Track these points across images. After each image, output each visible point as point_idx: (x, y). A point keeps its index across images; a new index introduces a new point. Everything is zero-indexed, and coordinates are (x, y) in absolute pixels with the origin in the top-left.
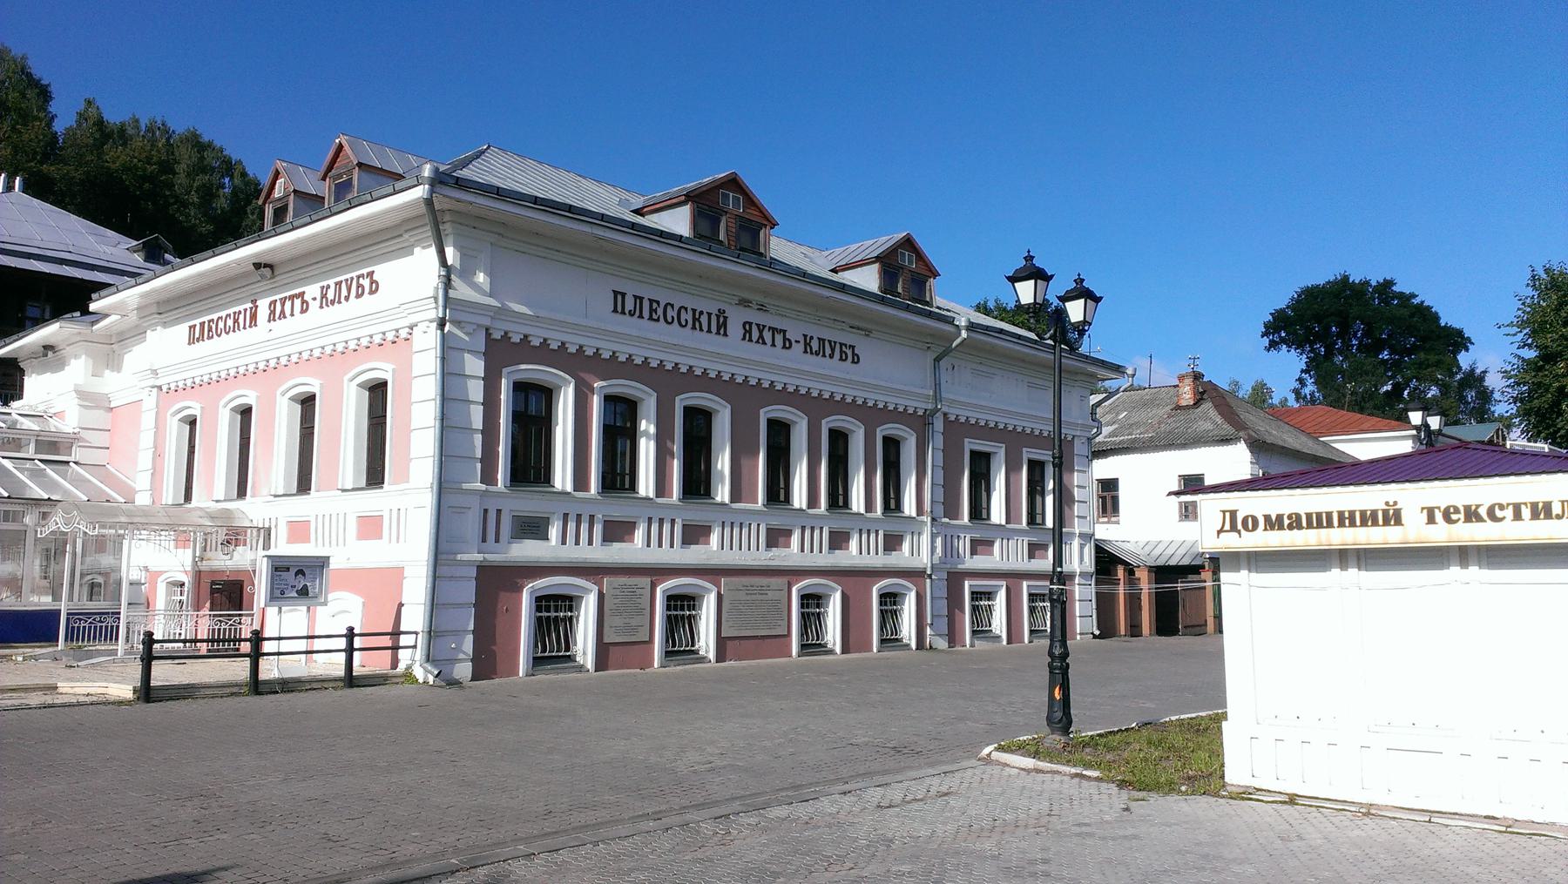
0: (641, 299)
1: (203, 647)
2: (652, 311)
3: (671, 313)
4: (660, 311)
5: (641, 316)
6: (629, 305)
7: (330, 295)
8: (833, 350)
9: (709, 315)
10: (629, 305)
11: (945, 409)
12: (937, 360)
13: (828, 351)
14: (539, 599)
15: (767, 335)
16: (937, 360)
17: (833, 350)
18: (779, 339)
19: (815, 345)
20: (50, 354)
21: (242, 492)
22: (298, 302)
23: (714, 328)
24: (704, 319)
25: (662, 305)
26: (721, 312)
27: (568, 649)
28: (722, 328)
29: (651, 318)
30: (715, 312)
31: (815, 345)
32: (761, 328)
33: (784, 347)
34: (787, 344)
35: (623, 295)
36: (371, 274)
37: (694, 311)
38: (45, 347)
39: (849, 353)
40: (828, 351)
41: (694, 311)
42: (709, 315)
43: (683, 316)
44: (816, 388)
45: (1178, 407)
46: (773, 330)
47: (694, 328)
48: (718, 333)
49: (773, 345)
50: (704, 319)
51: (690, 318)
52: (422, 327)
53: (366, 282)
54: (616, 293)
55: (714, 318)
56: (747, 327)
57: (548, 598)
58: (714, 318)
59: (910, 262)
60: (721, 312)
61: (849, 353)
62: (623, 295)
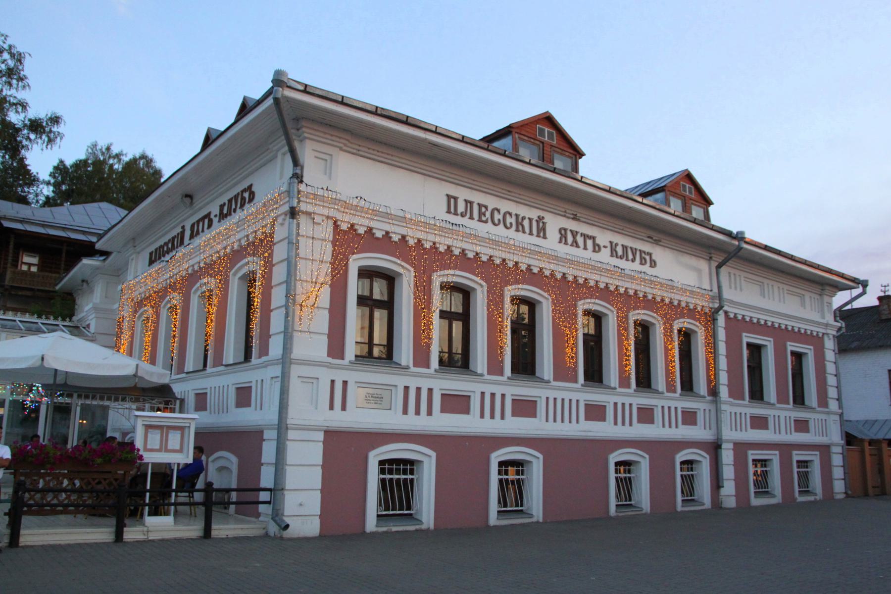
0: (471, 203)
1: (234, 496)
2: (481, 214)
3: (497, 217)
4: (488, 214)
5: (471, 218)
6: (461, 208)
7: (225, 211)
8: (634, 255)
9: (530, 220)
10: (461, 208)
11: (726, 308)
12: (719, 267)
13: (630, 257)
14: (381, 463)
15: (580, 240)
16: (719, 267)
17: (634, 255)
18: (589, 243)
19: (620, 250)
20: (85, 284)
21: (137, 365)
22: (206, 221)
23: (535, 231)
24: (526, 223)
25: (490, 209)
26: (540, 219)
27: (409, 508)
28: (542, 231)
29: (480, 220)
30: (536, 218)
31: (620, 250)
32: (574, 234)
33: (594, 251)
34: (597, 248)
35: (456, 199)
36: (250, 187)
37: (517, 215)
38: (83, 281)
39: (648, 258)
40: (630, 257)
41: (517, 215)
42: (530, 220)
43: (509, 220)
44: (624, 285)
45: (883, 321)
46: (586, 237)
47: (517, 230)
48: (538, 236)
49: (585, 248)
50: (526, 223)
51: (513, 220)
52: (280, 220)
53: (246, 195)
54: (447, 195)
55: (534, 224)
56: (563, 232)
57: (391, 462)
58: (534, 224)
59: (690, 192)
60: (540, 219)
61: (648, 258)
62: (456, 199)
